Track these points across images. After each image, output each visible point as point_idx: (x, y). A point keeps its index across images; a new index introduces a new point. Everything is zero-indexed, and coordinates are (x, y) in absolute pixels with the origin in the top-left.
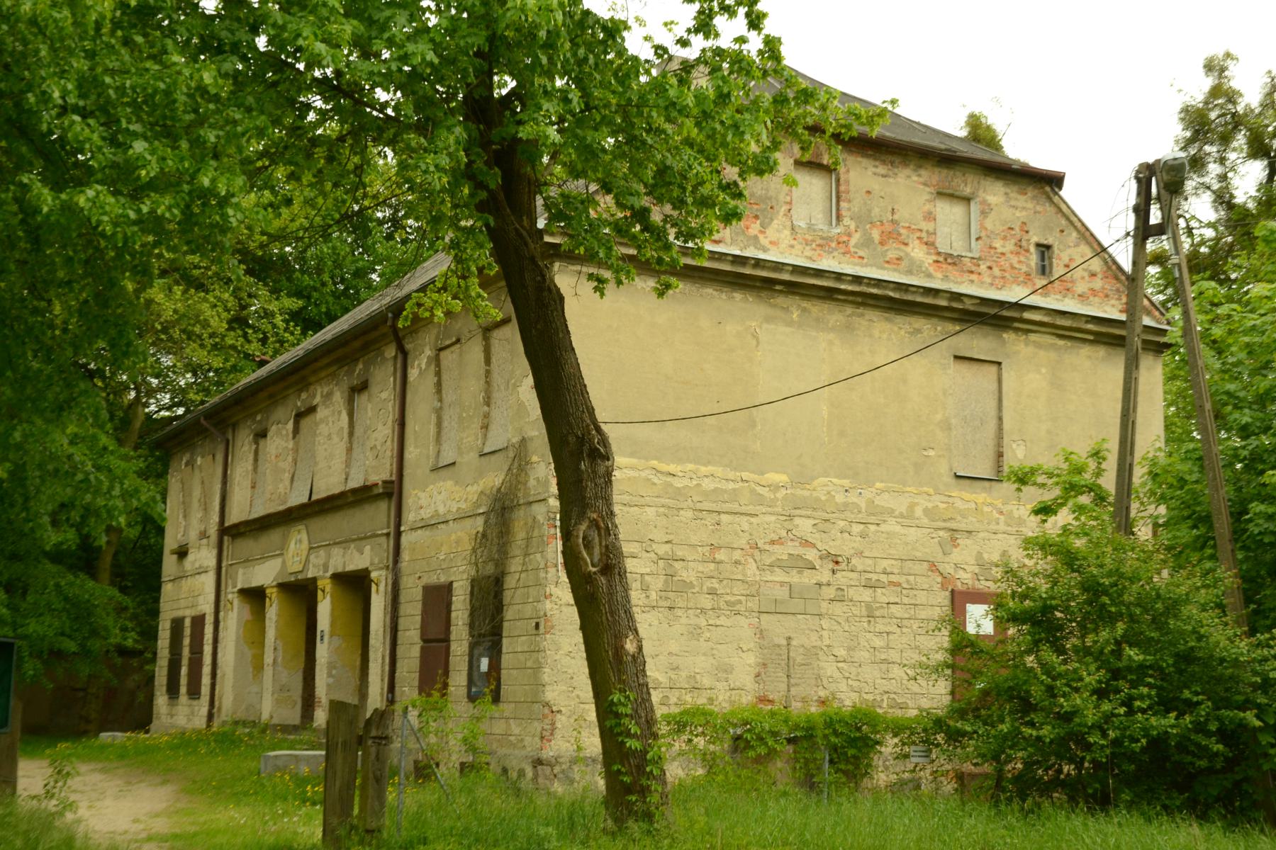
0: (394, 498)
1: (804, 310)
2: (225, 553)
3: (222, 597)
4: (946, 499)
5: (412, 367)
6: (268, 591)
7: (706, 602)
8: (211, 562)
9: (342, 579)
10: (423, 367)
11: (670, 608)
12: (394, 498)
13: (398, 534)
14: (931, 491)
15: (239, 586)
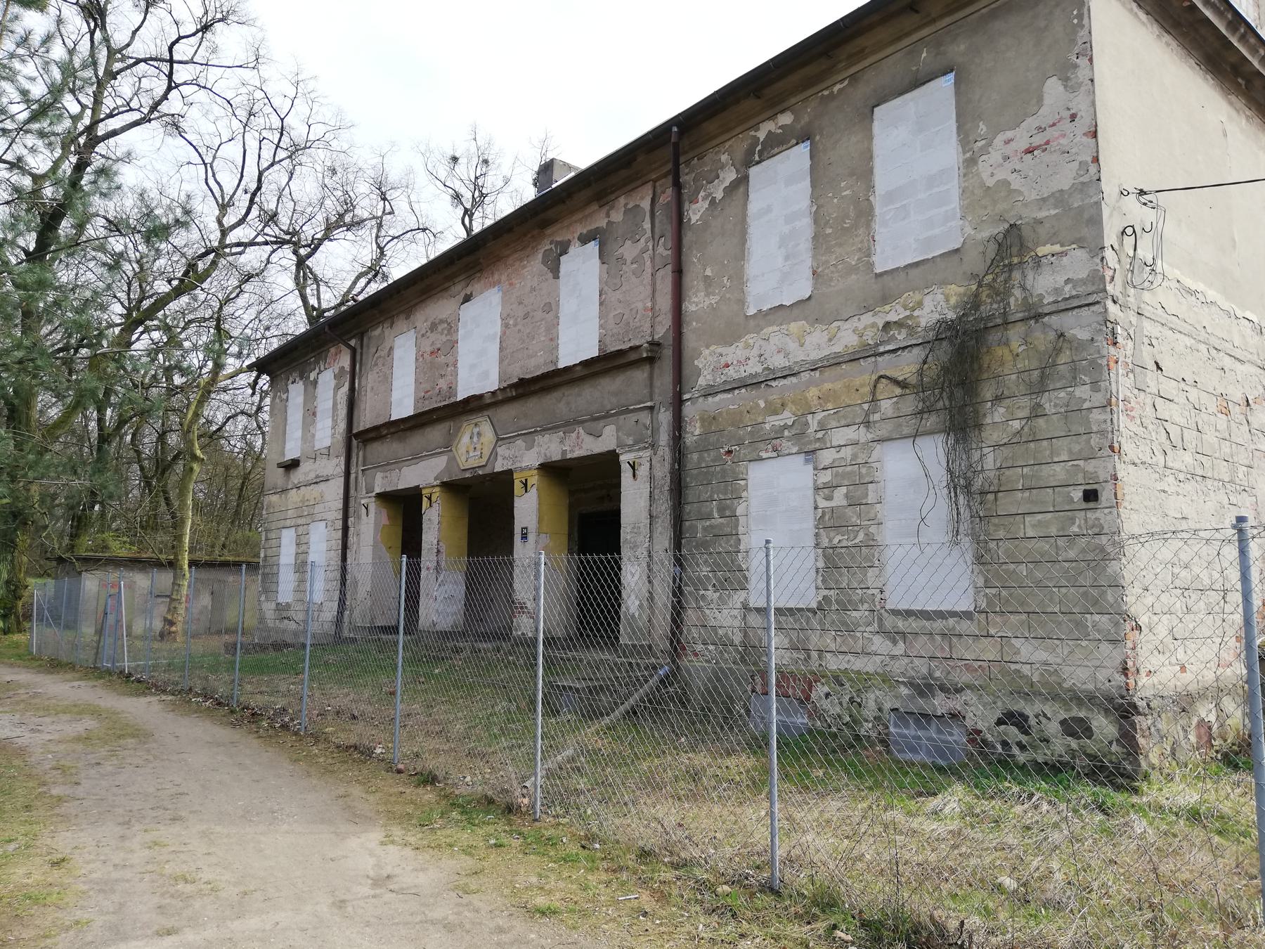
2: (354, 459)
3: (352, 503)
10: (719, 195)
13: (678, 403)
15: (378, 490)
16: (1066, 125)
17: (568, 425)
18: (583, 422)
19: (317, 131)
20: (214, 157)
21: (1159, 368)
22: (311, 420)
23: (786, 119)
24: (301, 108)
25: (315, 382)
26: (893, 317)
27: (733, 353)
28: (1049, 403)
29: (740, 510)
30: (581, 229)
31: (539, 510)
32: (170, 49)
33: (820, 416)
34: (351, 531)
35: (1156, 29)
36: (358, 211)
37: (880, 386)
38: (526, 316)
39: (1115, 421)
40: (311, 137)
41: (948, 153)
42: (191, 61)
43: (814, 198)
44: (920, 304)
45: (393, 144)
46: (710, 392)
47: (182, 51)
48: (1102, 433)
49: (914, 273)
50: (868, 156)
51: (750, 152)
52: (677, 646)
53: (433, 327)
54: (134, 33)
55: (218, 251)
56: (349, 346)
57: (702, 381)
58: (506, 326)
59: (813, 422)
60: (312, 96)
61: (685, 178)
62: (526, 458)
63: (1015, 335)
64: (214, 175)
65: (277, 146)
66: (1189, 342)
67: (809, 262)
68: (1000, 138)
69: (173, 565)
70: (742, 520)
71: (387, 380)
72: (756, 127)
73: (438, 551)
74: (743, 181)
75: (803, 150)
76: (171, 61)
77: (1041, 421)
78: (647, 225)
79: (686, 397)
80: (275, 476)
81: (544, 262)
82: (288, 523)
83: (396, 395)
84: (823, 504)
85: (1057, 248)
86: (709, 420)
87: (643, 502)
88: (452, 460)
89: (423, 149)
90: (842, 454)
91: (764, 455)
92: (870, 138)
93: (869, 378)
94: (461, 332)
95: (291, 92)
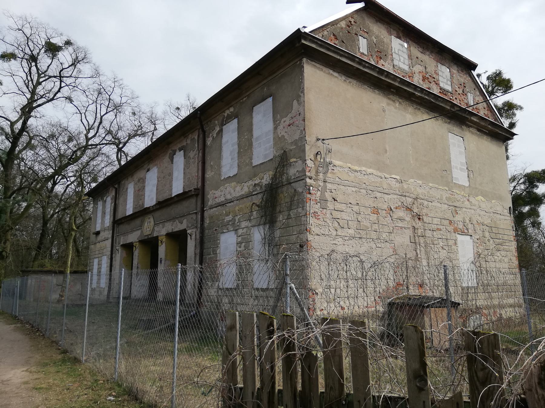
0: (200, 197)
1: (400, 103)
2: (115, 231)
3: (114, 249)
4: (452, 193)
5: (209, 137)
6: (134, 244)
7: (374, 235)
8: (110, 236)
9: (171, 236)
10: (215, 135)
11: (360, 238)
12: (200, 196)
13: (203, 211)
14: (447, 189)
15: (121, 243)
16: (298, 117)
17: (172, 219)
18: (178, 218)
19: (124, 100)
20: (86, 111)
21: (335, 200)
22: (102, 217)
23: (232, 109)
24: (117, 91)
25: (105, 201)
26: (257, 182)
27: (218, 193)
28: (292, 214)
29: (218, 252)
30: (179, 146)
31: (166, 251)
32: (60, 73)
33: (238, 217)
34: (114, 259)
35: (344, 78)
36: (144, 130)
37: (253, 207)
38: (164, 177)
39: (308, 221)
40: (122, 102)
41: (270, 126)
42: (71, 76)
43: (239, 138)
44: (263, 178)
45: (156, 103)
46: (211, 208)
47: (64, 73)
48: (304, 224)
49: (262, 166)
50: (251, 124)
51: (223, 121)
52: (199, 303)
53: (139, 181)
54: (48, 67)
55: (86, 147)
56: (115, 188)
57: (209, 204)
58: (158, 181)
59: (237, 219)
60: (122, 86)
61: (206, 129)
62: (162, 231)
63: (285, 189)
64: (86, 117)
65: (108, 107)
66: (354, 189)
67: (237, 161)
68: (283, 120)
69: (62, 273)
70: (218, 255)
71: (125, 201)
72: (224, 112)
73: (138, 267)
74: (221, 131)
75: (236, 121)
76: (60, 77)
77: (290, 220)
78: (196, 145)
79: (205, 209)
80: (93, 237)
81: (169, 158)
82: (96, 256)
83: (128, 206)
84: (239, 249)
85: (295, 160)
86: (211, 217)
87: (193, 249)
88: (142, 232)
89: (169, 104)
90: (244, 231)
91: (225, 231)
92: (252, 118)
93: (249, 204)
94: (146, 183)
95: (113, 85)
